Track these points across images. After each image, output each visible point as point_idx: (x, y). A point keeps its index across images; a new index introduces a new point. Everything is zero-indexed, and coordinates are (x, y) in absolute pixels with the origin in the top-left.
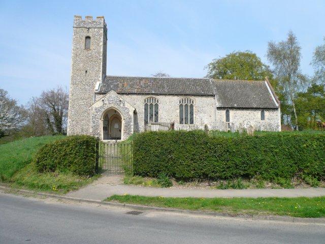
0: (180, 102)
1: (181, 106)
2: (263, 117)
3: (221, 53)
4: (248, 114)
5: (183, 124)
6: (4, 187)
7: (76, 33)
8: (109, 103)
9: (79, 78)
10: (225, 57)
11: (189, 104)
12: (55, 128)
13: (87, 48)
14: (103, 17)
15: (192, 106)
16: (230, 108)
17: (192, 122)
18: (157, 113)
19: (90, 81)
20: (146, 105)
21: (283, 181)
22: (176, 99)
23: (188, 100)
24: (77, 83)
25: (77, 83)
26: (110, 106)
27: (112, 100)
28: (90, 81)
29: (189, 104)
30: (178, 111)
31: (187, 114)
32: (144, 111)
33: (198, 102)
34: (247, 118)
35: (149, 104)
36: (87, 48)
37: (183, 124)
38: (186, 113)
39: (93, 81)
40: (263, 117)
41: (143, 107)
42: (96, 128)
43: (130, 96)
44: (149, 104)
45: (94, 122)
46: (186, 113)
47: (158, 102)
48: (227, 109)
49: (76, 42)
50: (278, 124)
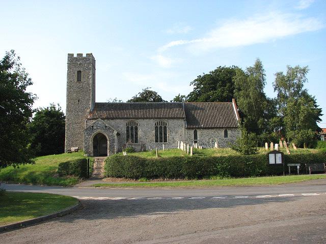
1: (156, 128)
15: (165, 128)
22: (152, 123)
26: (98, 131)
30: (154, 132)
38: (161, 134)
46: (161, 134)
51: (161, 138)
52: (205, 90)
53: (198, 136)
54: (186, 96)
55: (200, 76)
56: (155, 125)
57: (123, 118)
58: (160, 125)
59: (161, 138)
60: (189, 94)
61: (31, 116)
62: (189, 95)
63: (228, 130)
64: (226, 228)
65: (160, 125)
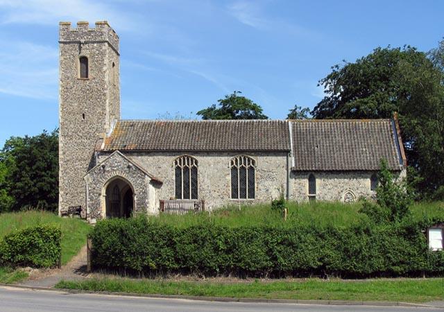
1: (234, 169)
3: (355, 52)
7: (64, 52)
9: (72, 126)
10: (355, 62)
12: (20, 257)
13: (85, 75)
14: (106, 23)
15: (252, 169)
16: (316, 171)
17: (252, 195)
18: (195, 182)
20: (178, 169)
22: (225, 162)
23: (245, 159)
24: (70, 134)
25: (70, 134)
26: (114, 174)
30: (229, 178)
31: (243, 183)
32: (174, 178)
33: (261, 162)
35: (182, 167)
36: (85, 75)
38: (243, 180)
41: (174, 172)
42: (257, 159)
44: (182, 167)
45: (91, 200)
46: (243, 180)
48: (312, 176)
49: (66, 67)
51: (243, 190)
52: (347, 96)
53: (317, 187)
54: (312, 110)
55: (337, 66)
56: (232, 163)
57: (220, 153)
58: (241, 164)
59: (243, 190)
60: (316, 105)
61: (342, 93)
62: (316, 108)
63: (316, 176)
64: (242, 292)
65: (241, 164)
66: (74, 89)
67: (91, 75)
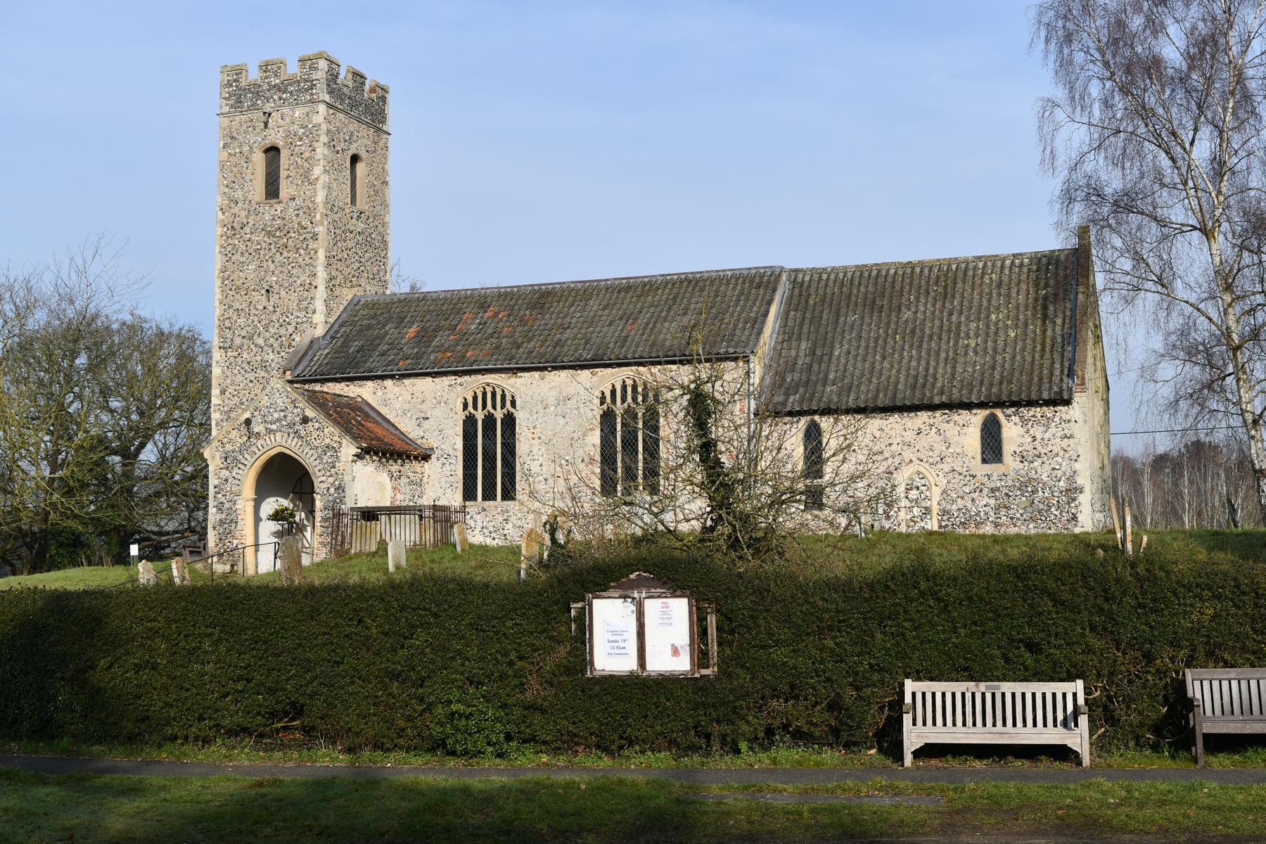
0: (465, 406)
2: (992, 447)
4: (910, 436)
5: (494, 499)
6: (529, 776)
8: (270, 431)
9: (241, 321)
11: (499, 415)
19: (283, 331)
20: (470, 422)
21: (855, 749)
24: (238, 341)
27: (278, 420)
28: (283, 331)
29: (499, 415)
30: (595, 438)
34: (908, 455)
37: (494, 499)
39: (291, 329)
40: (992, 447)
43: (407, 382)
47: (513, 404)
50: (1071, 479)
66: (247, 229)
67: (285, 190)
